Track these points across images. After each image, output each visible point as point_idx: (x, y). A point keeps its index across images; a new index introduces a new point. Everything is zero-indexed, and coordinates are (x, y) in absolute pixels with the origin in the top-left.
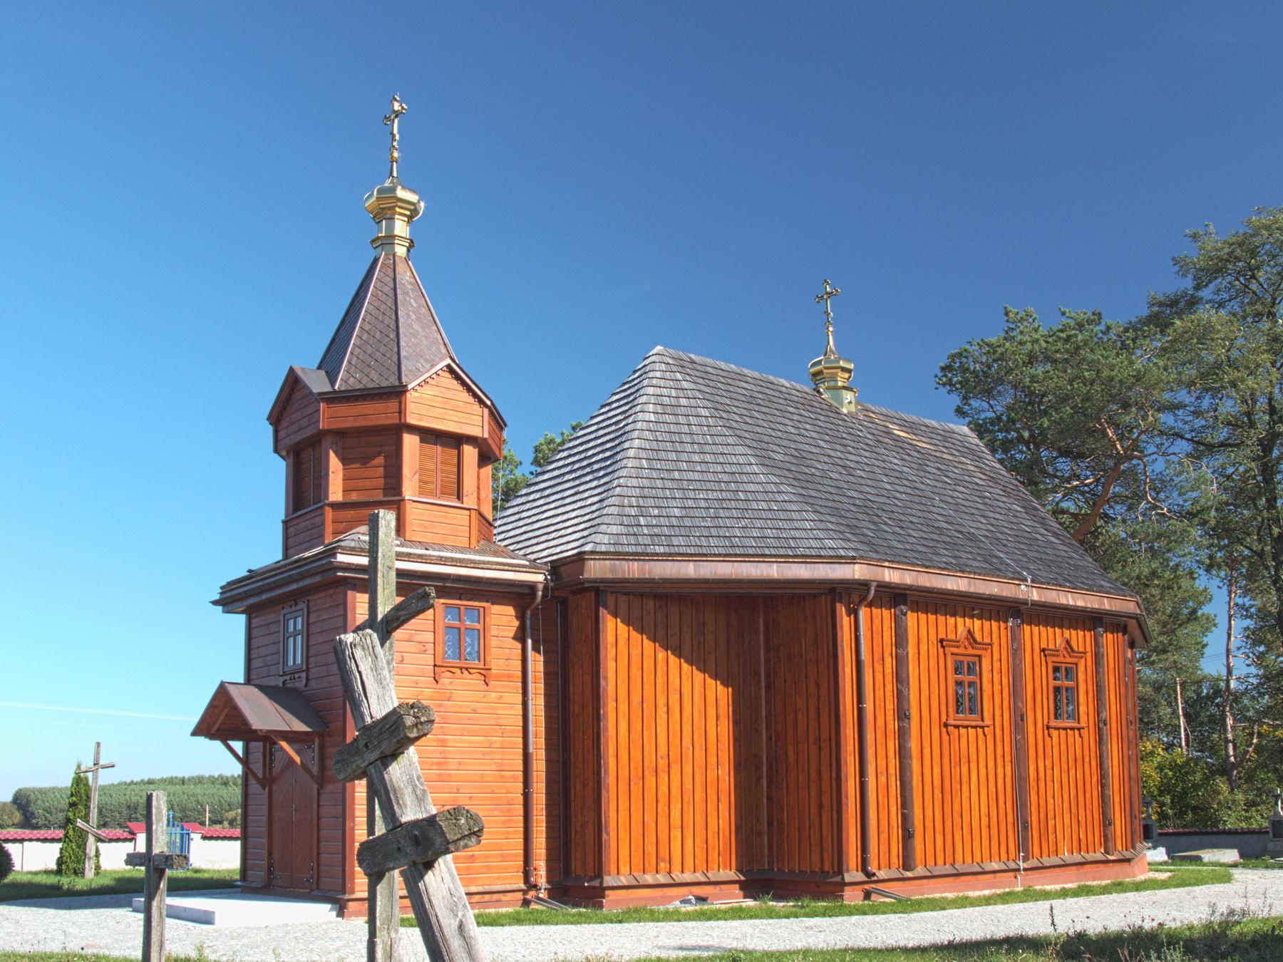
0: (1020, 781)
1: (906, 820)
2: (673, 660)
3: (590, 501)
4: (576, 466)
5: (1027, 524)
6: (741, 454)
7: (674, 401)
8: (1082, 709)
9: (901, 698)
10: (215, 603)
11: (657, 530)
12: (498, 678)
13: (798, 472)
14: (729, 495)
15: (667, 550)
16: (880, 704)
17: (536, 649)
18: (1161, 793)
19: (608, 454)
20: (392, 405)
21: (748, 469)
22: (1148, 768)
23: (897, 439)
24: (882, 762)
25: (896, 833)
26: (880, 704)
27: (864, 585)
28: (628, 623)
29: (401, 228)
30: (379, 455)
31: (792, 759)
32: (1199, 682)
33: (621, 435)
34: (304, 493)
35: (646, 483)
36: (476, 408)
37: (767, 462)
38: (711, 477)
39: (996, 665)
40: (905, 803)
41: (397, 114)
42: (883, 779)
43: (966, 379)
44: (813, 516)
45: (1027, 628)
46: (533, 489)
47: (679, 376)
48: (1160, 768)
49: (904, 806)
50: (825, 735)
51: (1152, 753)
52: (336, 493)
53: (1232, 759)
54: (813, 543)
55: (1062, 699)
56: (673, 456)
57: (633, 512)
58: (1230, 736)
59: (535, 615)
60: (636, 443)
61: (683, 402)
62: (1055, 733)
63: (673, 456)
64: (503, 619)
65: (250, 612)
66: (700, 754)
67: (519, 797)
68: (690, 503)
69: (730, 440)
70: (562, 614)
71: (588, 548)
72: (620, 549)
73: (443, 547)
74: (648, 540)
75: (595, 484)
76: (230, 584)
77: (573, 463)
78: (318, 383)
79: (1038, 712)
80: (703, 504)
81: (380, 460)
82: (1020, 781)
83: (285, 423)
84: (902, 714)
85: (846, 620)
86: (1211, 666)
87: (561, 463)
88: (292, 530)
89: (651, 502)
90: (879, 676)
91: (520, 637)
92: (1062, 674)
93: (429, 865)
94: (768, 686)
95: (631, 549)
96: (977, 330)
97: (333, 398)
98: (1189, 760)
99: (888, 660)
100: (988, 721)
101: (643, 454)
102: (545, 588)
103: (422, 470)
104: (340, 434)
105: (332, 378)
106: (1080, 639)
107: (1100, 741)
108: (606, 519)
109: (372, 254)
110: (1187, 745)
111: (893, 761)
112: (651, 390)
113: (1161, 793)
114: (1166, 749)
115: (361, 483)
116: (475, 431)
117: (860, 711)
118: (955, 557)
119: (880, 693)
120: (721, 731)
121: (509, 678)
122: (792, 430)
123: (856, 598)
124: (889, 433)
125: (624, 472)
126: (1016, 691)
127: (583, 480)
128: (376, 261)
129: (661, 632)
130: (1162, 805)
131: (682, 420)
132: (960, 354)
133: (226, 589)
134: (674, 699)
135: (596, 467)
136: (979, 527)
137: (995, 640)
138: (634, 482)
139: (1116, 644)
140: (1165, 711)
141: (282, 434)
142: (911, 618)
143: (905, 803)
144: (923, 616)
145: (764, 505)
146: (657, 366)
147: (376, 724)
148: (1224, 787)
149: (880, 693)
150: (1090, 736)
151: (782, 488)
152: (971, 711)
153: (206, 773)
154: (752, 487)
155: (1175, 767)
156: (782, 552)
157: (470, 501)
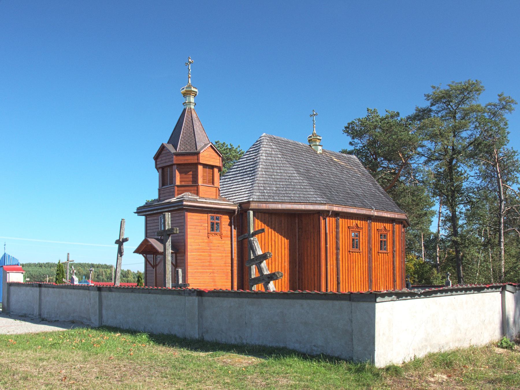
0: (370, 269)
1: (338, 279)
2: (273, 232)
3: (248, 184)
4: (241, 171)
5: (373, 189)
6: (291, 170)
7: (270, 152)
8: (388, 247)
9: (337, 243)
10: (135, 213)
11: (270, 194)
12: (225, 237)
13: (307, 175)
14: (288, 183)
15: (273, 200)
16: (331, 245)
17: (235, 228)
18: (414, 274)
19: (252, 169)
20: (196, 157)
21: (294, 175)
22: (411, 265)
23: (334, 162)
24: (332, 262)
25: (335, 282)
26: (331, 245)
27: (328, 211)
28: (261, 221)
29: (192, 99)
30: (191, 171)
31: (306, 260)
32: (430, 234)
33: (256, 163)
34: (166, 180)
35: (265, 179)
36: (218, 157)
37: (299, 172)
38: (283, 177)
39: (364, 234)
40: (338, 274)
41: (190, 63)
42: (332, 267)
43: (353, 131)
44: (313, 190)
45: (373, 223)
46: (226, 177)
47: (271, 144)
48: (415, 265)
49: (337, 275)
50: (316, 254)
51: (412, 260)
52: (178, 183)
53: (438, 262)
54: (314, 199)
55: (383, 244)
56: (272, 170)
57: (262, 188)
58: (438, 255)
59: (234, 219)
60: (261, 166)
61: (273, 152)
62: (380, 254)
63: (272, 170)
64: (225, 220)
65: (146, 216)
66: (280, 259)
67: (230, 271)
68: (278, 186)
69: (288, 166)
70: (239, 217)
71: (251, 200)
72: (260, 200)
73: (210, 199)
74: (267, 197)
75: (249, 178)
76: (140, 207)
77: (240, 170)
78: (171, 148)
79: (376, 248)
80: (282, 186)
81: (191, 173)
82: (370, 269)
83: (159, 160)
84: (337, 249)
85: (322, 221)
86: (433, 229)
87: (235, 170)
88: (162, 192)
89: (267, 185)
90: (331, 237)
91: (230, 225)
92: (383, 237)
93: (269, 283)
94: (299, 239)
95: (263, 200)
96: (358, 114)
97: (177, 155)
98: (425, 262)
99: (334, 232)
100: (361, 251)
101: (263, 170)
102: (238, 211)
103: (203, 176)
104: (178, 165)
105: (175, 147)
106: (388, 226)
107: (393, 257)
108: (255, 191)
109: (183, 108)
110: (424, 256)
111: (335, 262)
112: (263, 149)
113: (414, 274)
114: (417, 258)
115: (185, 179)
116: (218, 165)
117: (326, 247)
118: (353, 202)
119: (331, 242)
120: (286, 252)
121: (227, 237)
122: (304, 161)
123: (325, 215)
124: (332, 160)
125: (258, 176)
126: (369, 242)
127: (244, 176)
128: (185, 110)
129: (270, 224)
130: (415, 278)
131: (273, 159)
132: (352, 123)
133: (138, 209)
134: (273, 243)
135: (248, 173)
136: (359, 192)
137: (364, 227)
138: (261, 179)
139: (399, 228)
140: (417, 245)
141: (158, 163)
142: (340, 220)
143: (338, 274)
144: (344, 220)
145: (299, 187)
146: (265, 141)
147: (259, 256)
148: (436, 272)
149: (331, 242)
150: (390, 255)
151: (304, 181)
152: (357, 248)
153: (32, 262)
154: (295, 181)
155: (420, 264)
156: (305, 201)
157: (216, 185)
